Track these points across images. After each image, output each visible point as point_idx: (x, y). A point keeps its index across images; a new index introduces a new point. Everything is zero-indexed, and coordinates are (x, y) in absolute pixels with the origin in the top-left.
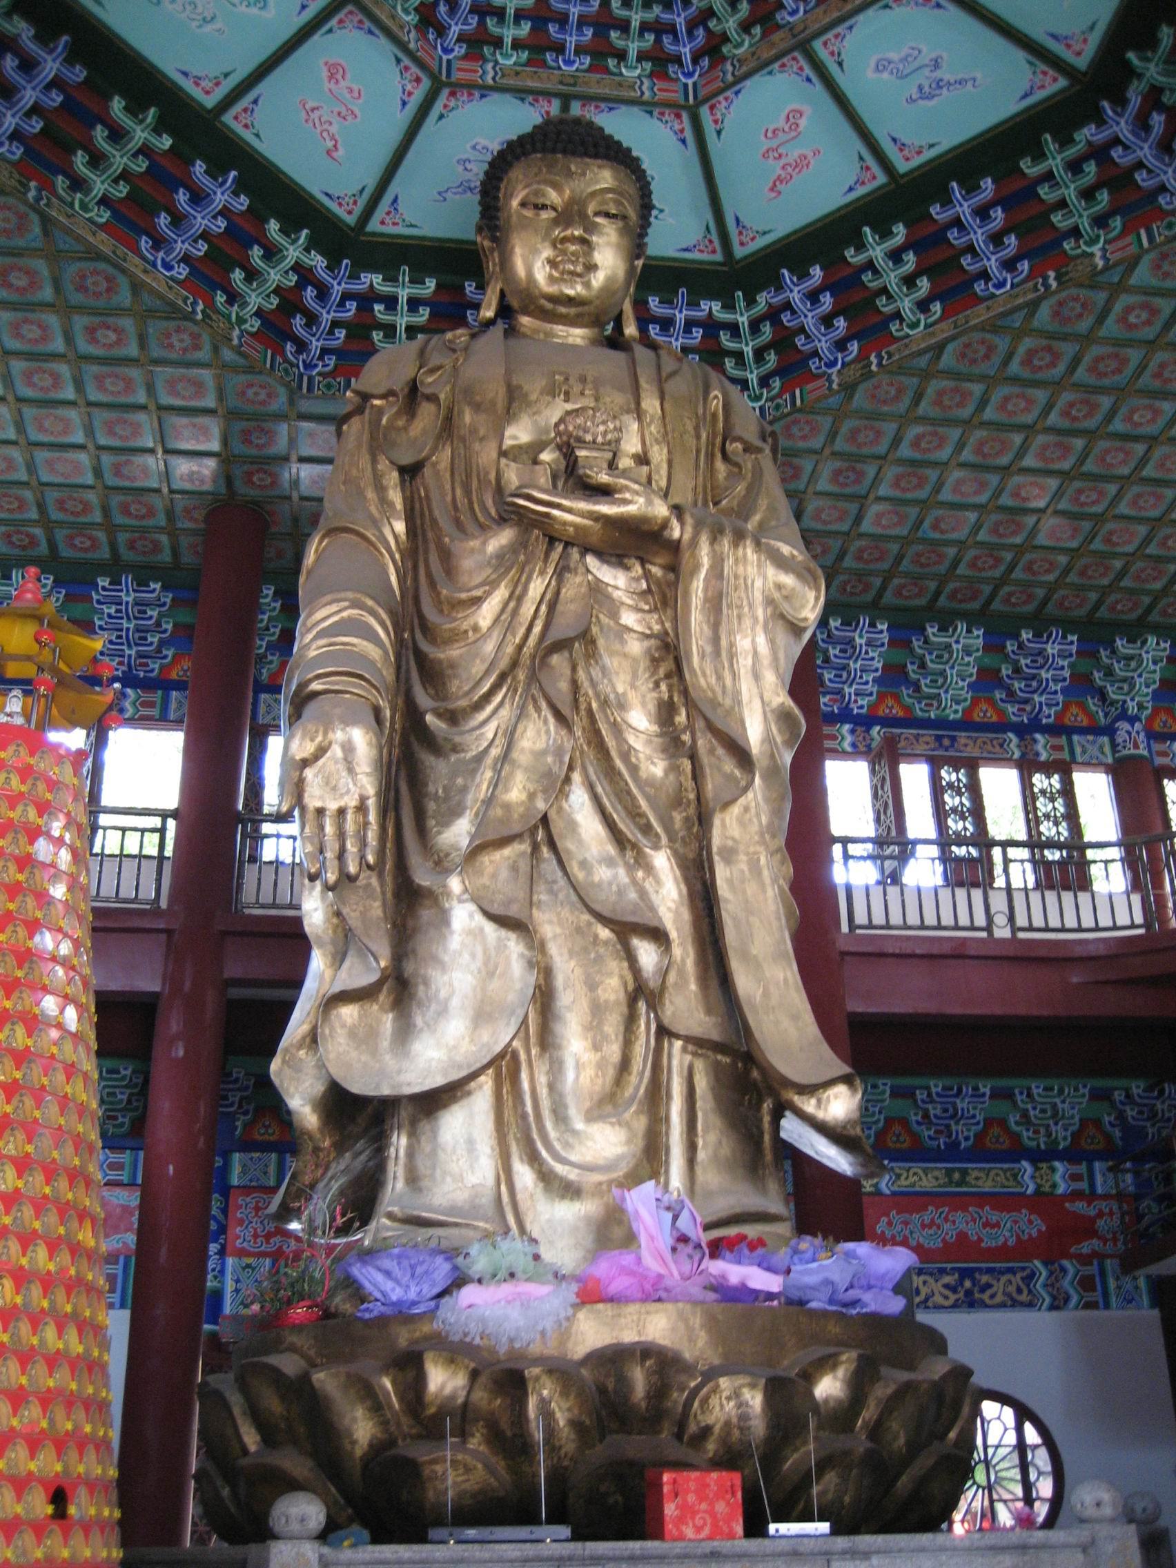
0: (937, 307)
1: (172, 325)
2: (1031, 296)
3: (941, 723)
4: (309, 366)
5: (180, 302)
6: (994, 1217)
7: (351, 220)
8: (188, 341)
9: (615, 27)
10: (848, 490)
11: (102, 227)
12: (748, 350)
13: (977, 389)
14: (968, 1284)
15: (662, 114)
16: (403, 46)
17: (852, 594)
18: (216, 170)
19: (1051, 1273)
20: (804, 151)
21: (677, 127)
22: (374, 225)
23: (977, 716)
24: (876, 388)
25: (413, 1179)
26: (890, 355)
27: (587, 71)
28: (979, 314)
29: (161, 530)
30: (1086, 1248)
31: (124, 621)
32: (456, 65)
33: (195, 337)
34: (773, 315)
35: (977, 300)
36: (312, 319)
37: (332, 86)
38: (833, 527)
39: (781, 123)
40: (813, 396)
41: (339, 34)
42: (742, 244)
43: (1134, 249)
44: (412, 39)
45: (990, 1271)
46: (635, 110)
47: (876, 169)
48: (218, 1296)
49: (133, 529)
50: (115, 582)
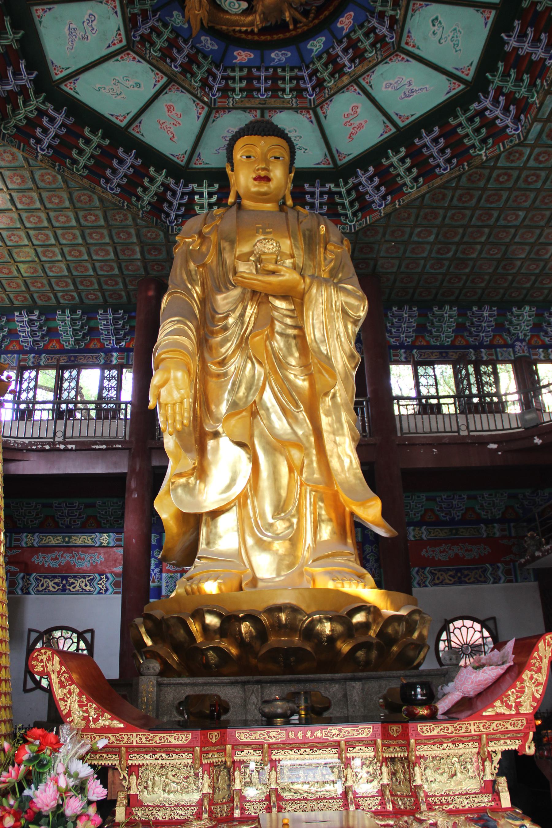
0: (421, 180)
2: (458, 173)
3: (442, 347)
4: (171, 222)
6: (469, 547)
7: (183, 164)
8: (122, 218)
10: (394, 255)
11: (85, 177)
12: (347, 202)
13: (441, 212)
14: (459, 575)
16: (195, 96)
19: (493, 569)
23: (457, 343)
25: (208, 544)
26: (403, 200)
28: (438, 182)
30: (508, 558)
32: (217, 100)
33: (125, 215)
34: (356, 187)
35: (436, 176)
36: (170, 204)
39: (350, 112)
43: (498, 152)
44: (199, 93)
45: (468, 569)
46: (290, 111)
47: (391, 126)
48: (159, 588)
50: (105, 311)
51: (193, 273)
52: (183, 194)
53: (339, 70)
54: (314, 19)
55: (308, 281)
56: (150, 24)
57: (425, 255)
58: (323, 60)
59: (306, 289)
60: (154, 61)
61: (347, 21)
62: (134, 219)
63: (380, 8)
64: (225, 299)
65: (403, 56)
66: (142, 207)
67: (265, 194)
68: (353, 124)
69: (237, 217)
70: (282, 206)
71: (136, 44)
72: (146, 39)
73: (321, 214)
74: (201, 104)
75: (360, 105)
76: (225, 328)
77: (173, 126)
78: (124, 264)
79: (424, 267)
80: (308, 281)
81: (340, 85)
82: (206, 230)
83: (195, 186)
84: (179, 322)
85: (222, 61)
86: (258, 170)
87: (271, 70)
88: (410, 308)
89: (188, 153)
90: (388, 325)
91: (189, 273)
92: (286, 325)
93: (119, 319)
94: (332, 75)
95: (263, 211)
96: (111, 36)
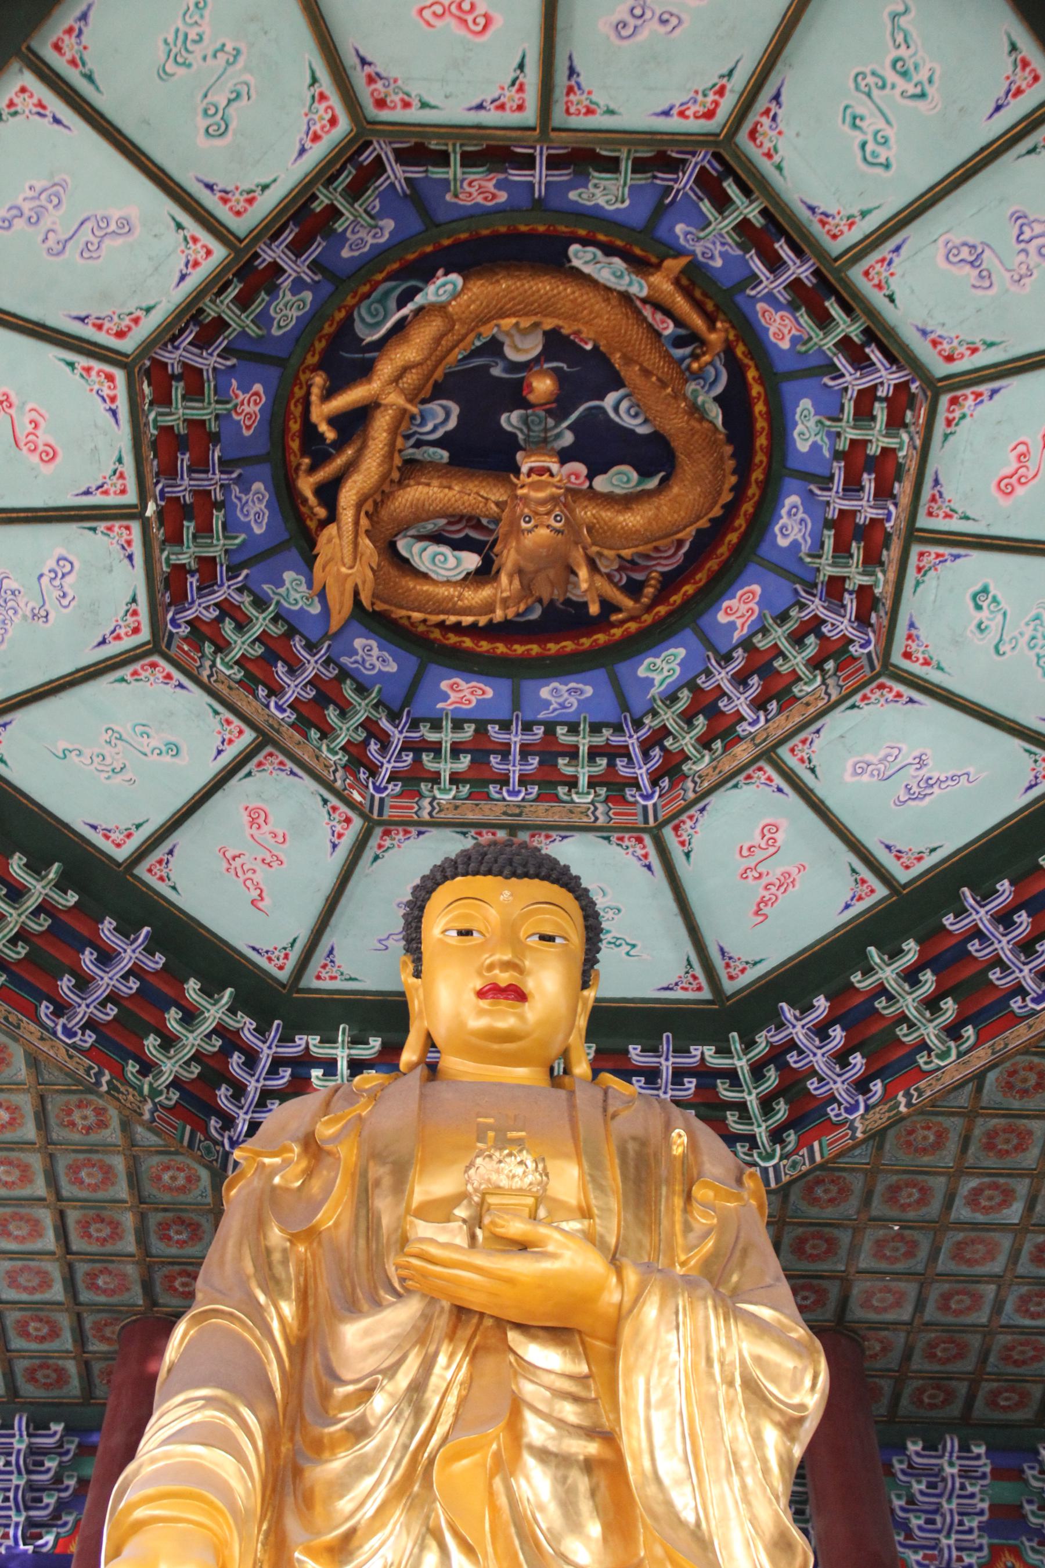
0: (969, 1032)
1: (74, 1098)
5: (81, 1072)
7: (283, 976)
8: (92, 1119)
9: (563, 755)
10: (899, 1267)
15: (621, 839)
17: (932, 1406)
18: (126, 930)
20: (787, 868)
21: (640, 852)
22: (309, 981)
24: (911, 1133)
27: (534, 801)
29: (65, 1354)
31: (14, 1477)
32: (388, 802)
33: (100, 1111)
34: (777, 1055)
35: (1017, 1019)
36: (239, 1090)
37: (254, 831)
38: (890, 1316)
39: (757, 839)
40: (837, 1148)
41: (258, 776)
42: (731, 978)
46: (590, 837)
49: (30, 1355)
51: (277, 1256)
52: (278, 1063)
53: (722, 731)
54: (656, 601)
55: (632, 1277)
56: (219, 596)
57: (997, 1266)
58: (681, 705)
59: (627, 1305)
60: (224, 691)
61: (743, 608)
62: (126, 1126)
63: (830, 571)
64: (367, 1332)
65: (898, 687)
66: (154, 1092)
67: (508, 1036)
68: (763, 875)
69: (422, 1096)
70: (558, 1076)
71: (176, 642)
72: (201, 633)
73: (677, 1103)
74: (343, 808)
75: (784, 823)
76: (360, 1431)
77: (263, 865)
78: (82, 1269)
79: (998, 1307)
80: (632, 1277)
81: (727, 767)
82: (326, 1131)
83: (314, 1040)
84: (209, 1401)
85: (408, 699)
86: (491, 967)
87: (539, 731)
88: (965, 1448)
89: (299, 947)
90: (897, 1503)
91: (264, 1257)
92: (560, 1423)
93: (45, 1452)
94: (705, 743)
95: (501, 1084)
96: (112, 612)
